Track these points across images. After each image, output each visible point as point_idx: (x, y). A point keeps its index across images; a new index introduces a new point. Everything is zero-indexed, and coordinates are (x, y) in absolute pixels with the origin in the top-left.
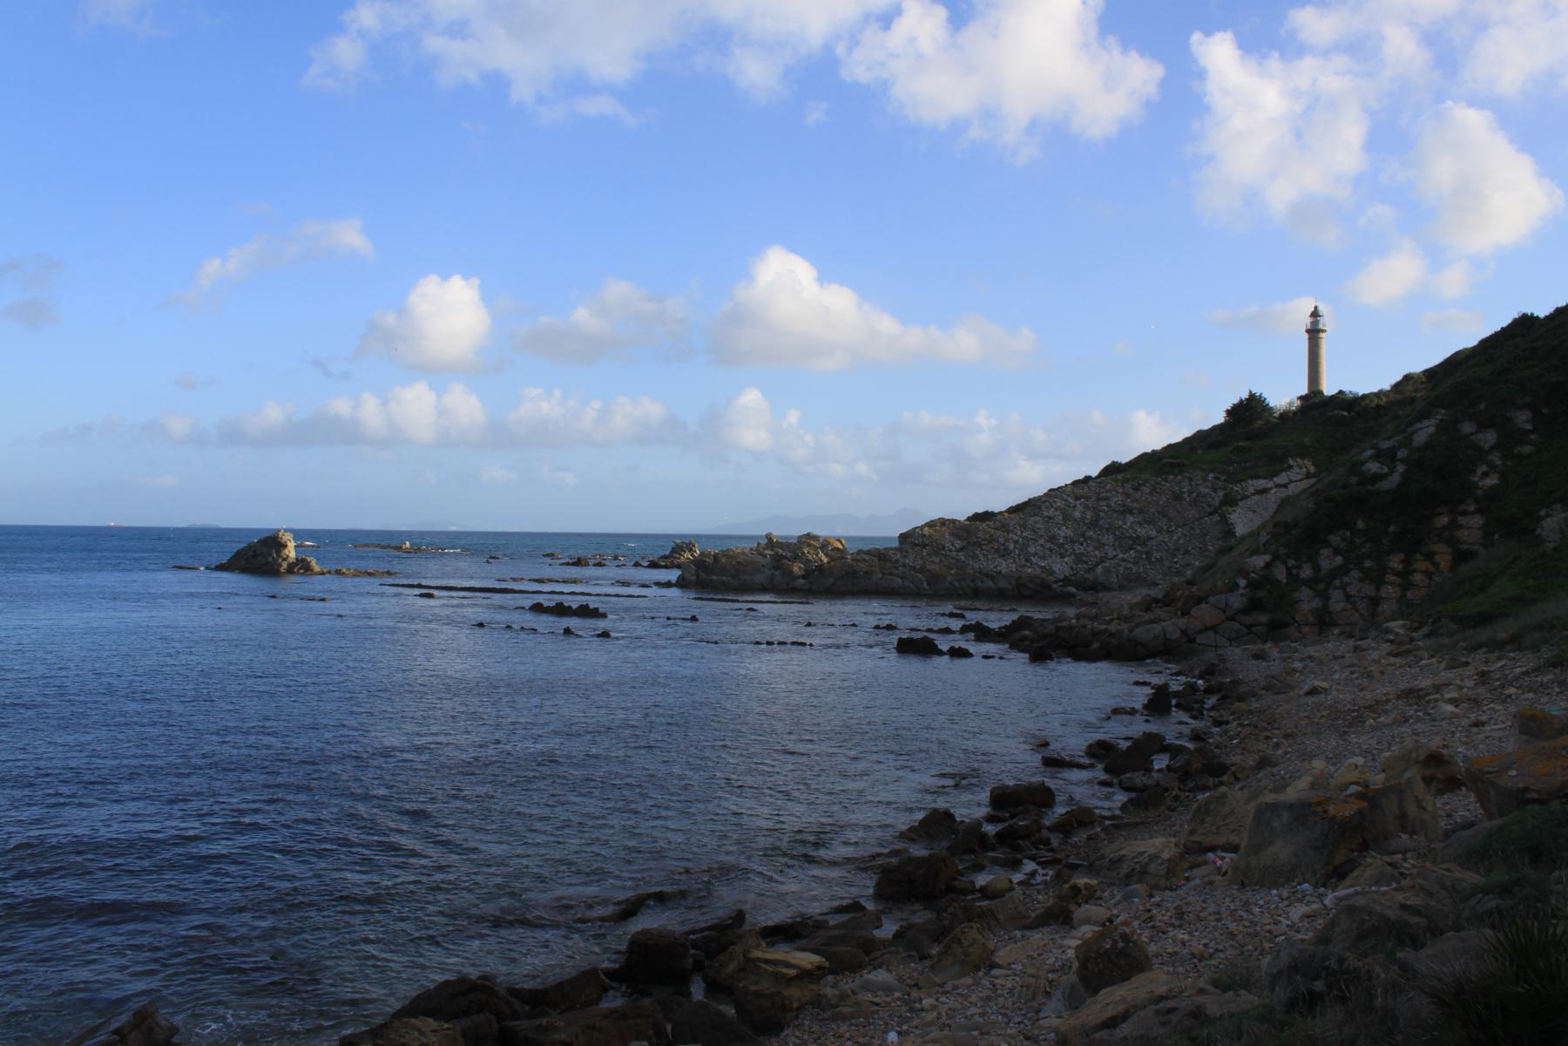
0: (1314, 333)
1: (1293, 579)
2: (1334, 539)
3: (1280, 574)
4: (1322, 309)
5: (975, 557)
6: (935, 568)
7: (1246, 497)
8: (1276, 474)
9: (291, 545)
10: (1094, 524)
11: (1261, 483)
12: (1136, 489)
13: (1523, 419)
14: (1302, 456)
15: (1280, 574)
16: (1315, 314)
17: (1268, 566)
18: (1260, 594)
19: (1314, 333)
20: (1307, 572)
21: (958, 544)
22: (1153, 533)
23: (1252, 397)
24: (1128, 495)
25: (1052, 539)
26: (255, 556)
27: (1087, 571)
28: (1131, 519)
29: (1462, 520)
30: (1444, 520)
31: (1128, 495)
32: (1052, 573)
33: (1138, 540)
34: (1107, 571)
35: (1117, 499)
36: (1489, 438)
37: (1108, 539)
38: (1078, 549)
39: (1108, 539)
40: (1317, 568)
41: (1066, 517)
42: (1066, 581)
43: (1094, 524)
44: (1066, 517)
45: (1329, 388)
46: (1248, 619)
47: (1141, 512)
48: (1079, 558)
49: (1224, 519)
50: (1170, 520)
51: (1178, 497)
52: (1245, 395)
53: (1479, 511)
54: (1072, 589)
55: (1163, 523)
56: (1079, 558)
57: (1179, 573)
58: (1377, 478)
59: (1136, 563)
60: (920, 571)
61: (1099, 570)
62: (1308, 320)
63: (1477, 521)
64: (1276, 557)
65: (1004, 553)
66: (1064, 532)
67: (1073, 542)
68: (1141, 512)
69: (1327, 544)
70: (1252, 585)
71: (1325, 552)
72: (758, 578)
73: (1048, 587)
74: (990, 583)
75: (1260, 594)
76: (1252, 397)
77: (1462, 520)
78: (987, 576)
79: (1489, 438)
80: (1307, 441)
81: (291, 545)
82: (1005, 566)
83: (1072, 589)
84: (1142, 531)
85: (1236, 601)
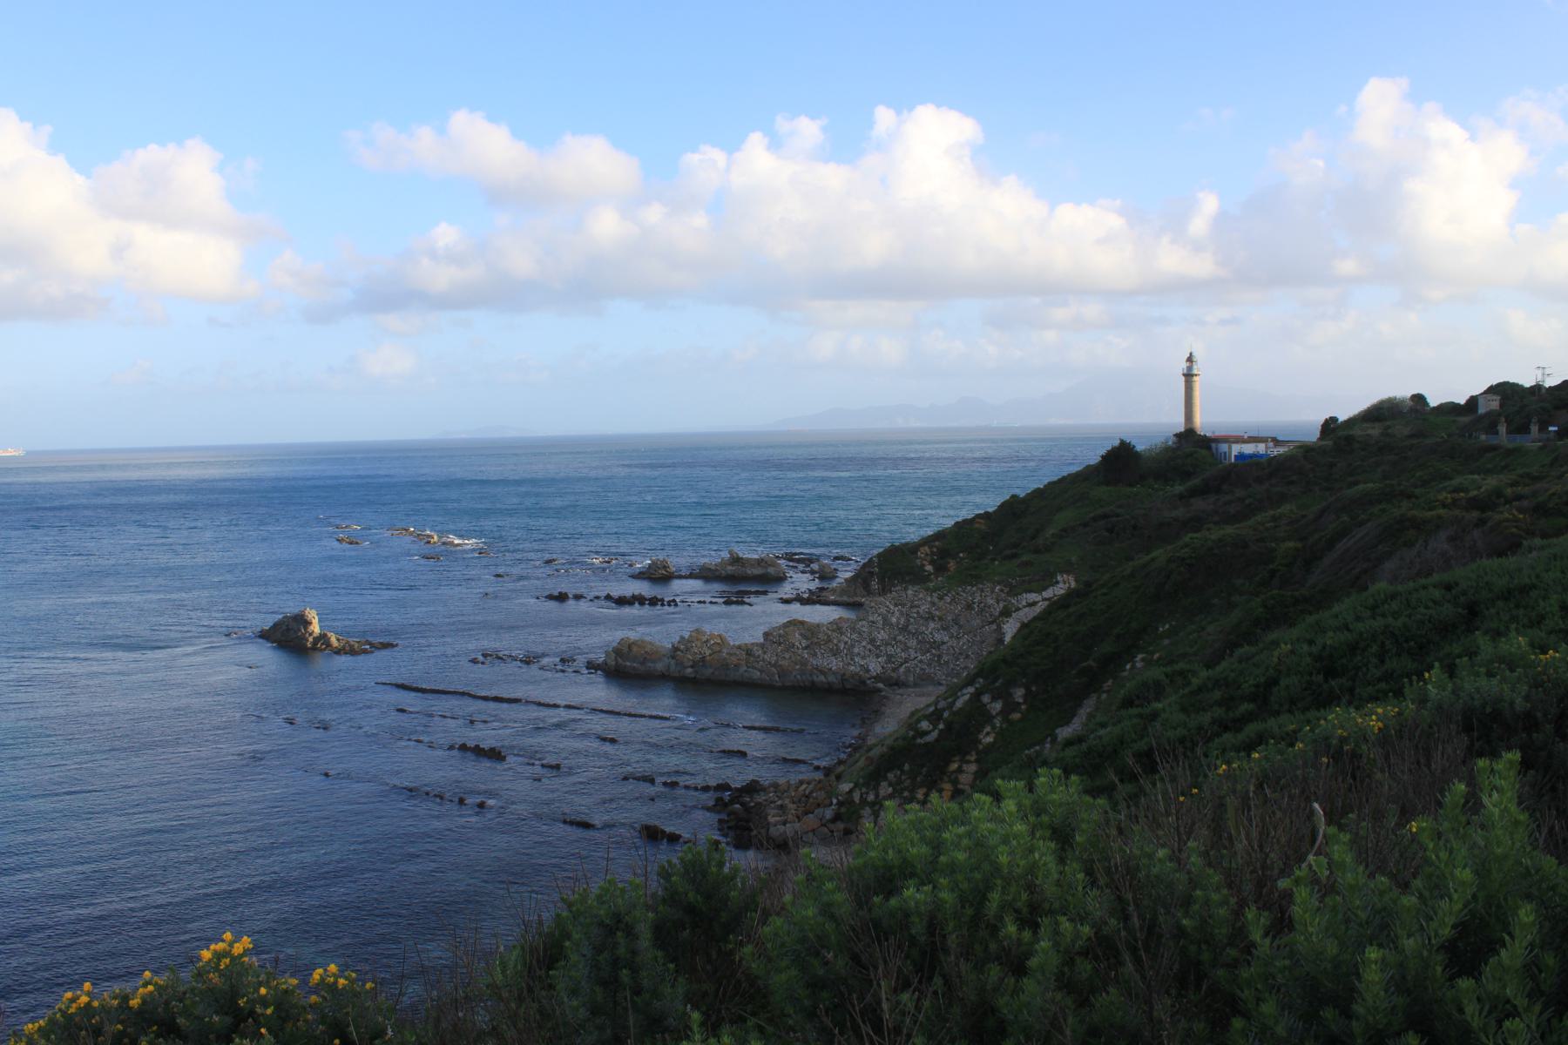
0: (1189, 376)
1: (863, 801)
2: (890, 776)
3: (856, 797)
4: (1197, 356)
5: (815, 655)
6: (784, 663)
7: (1018, 609)
8: (1045, 589)
9: (315, 621)
10: (904, 629)
11: (1033, 597)
12: (941, 598)
13: (1019, 694)
14: (1068, 572)
15: (856, 797)
16: (1190, 359)
17: (851, 791)
18: (843, 810)
19: (1189, 376)
20: (871, 797)
21: (804, 643)
22: (946, 639)
23: (1123, 443)
24: (933, 604)
25: (872, 641)
26: (288, 630)
27: (894, 670)
28: (932, 625)
29: (965, 767)
30: (954, 766)
31: (933, 604)
32: (868, 671)
33: (937, 645)
34: (908, 670)
35: (924, 608)
36: (997, 706)
37: (913, 643)
38: (890, 650)
39: (913, 643)
40: (877, 796)
41: (886, 621)
42: (878, 678)
43: (904, 629)
44: (886, 621)
45: (1204, 422)
46: (832, 826)
47: (940, 619)
48: (890, 658)
49: (999, 628)
50: (961, 627)
51: (969, 607)
52: (1117, 443)
53: (977, 761)
54: (880, 685)
55: (954, 630)
56: (890, 658)
57: (958, 675)
58: (926, 733)
59: (929, 665)
60: (775, 665)
61: (902, 670)
62: (1185, 365)
63: (973, 768)
64: (856, 785)
65: (836, 653)
66: (882, 635)
67: (887, 644)
68: (940, 619)
69: (886, 779)
70: (840, 804)
71: (884, 784)
72: (660, 666)
73: (864, 682)
74: (822, 678)
75: (843, 810)
76: (1123, 443)
77: (965, 767)
78: (822, 672)
79: (997, 706)
80: (1074, 559)
81: (315, 621)
82: (835, 664)
83: (880, 685)
84: (938, 637)
85: (829, 813)
